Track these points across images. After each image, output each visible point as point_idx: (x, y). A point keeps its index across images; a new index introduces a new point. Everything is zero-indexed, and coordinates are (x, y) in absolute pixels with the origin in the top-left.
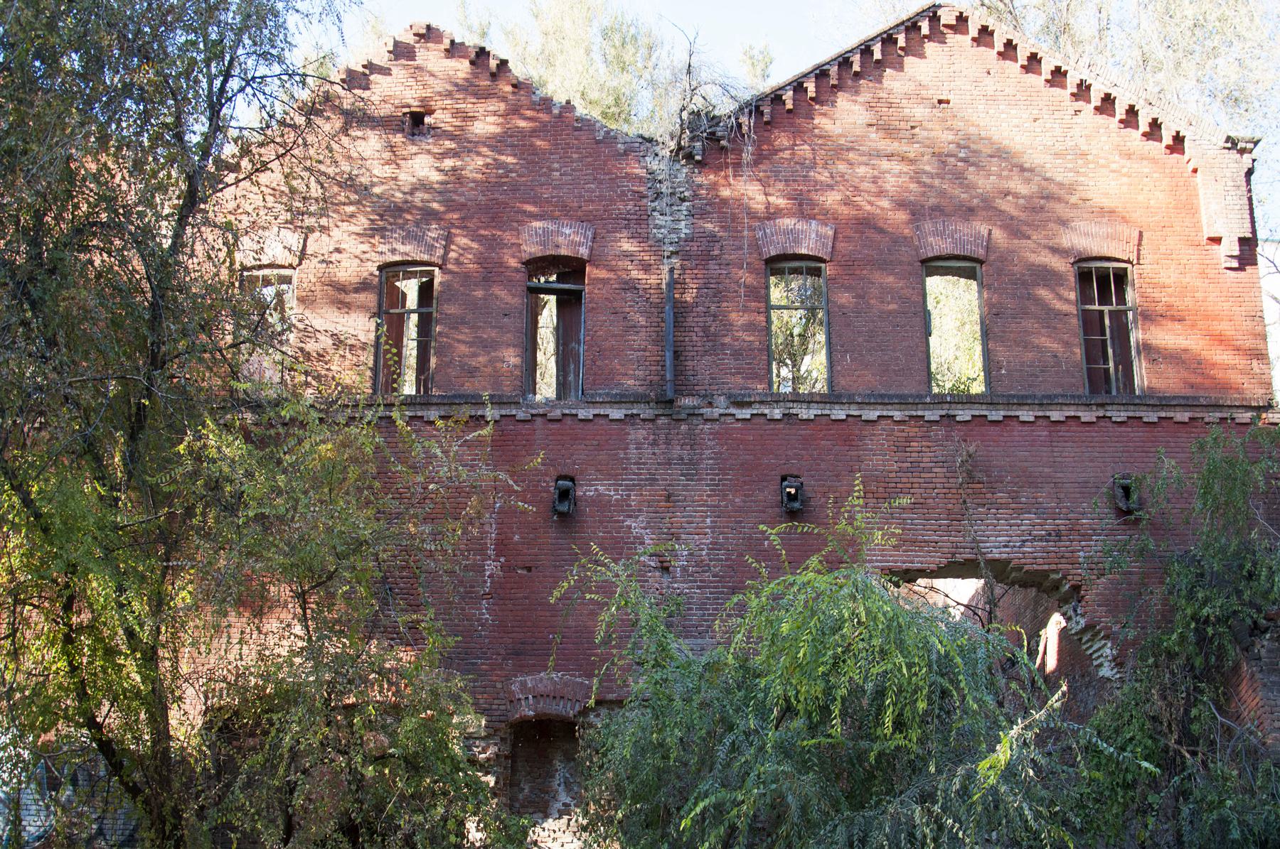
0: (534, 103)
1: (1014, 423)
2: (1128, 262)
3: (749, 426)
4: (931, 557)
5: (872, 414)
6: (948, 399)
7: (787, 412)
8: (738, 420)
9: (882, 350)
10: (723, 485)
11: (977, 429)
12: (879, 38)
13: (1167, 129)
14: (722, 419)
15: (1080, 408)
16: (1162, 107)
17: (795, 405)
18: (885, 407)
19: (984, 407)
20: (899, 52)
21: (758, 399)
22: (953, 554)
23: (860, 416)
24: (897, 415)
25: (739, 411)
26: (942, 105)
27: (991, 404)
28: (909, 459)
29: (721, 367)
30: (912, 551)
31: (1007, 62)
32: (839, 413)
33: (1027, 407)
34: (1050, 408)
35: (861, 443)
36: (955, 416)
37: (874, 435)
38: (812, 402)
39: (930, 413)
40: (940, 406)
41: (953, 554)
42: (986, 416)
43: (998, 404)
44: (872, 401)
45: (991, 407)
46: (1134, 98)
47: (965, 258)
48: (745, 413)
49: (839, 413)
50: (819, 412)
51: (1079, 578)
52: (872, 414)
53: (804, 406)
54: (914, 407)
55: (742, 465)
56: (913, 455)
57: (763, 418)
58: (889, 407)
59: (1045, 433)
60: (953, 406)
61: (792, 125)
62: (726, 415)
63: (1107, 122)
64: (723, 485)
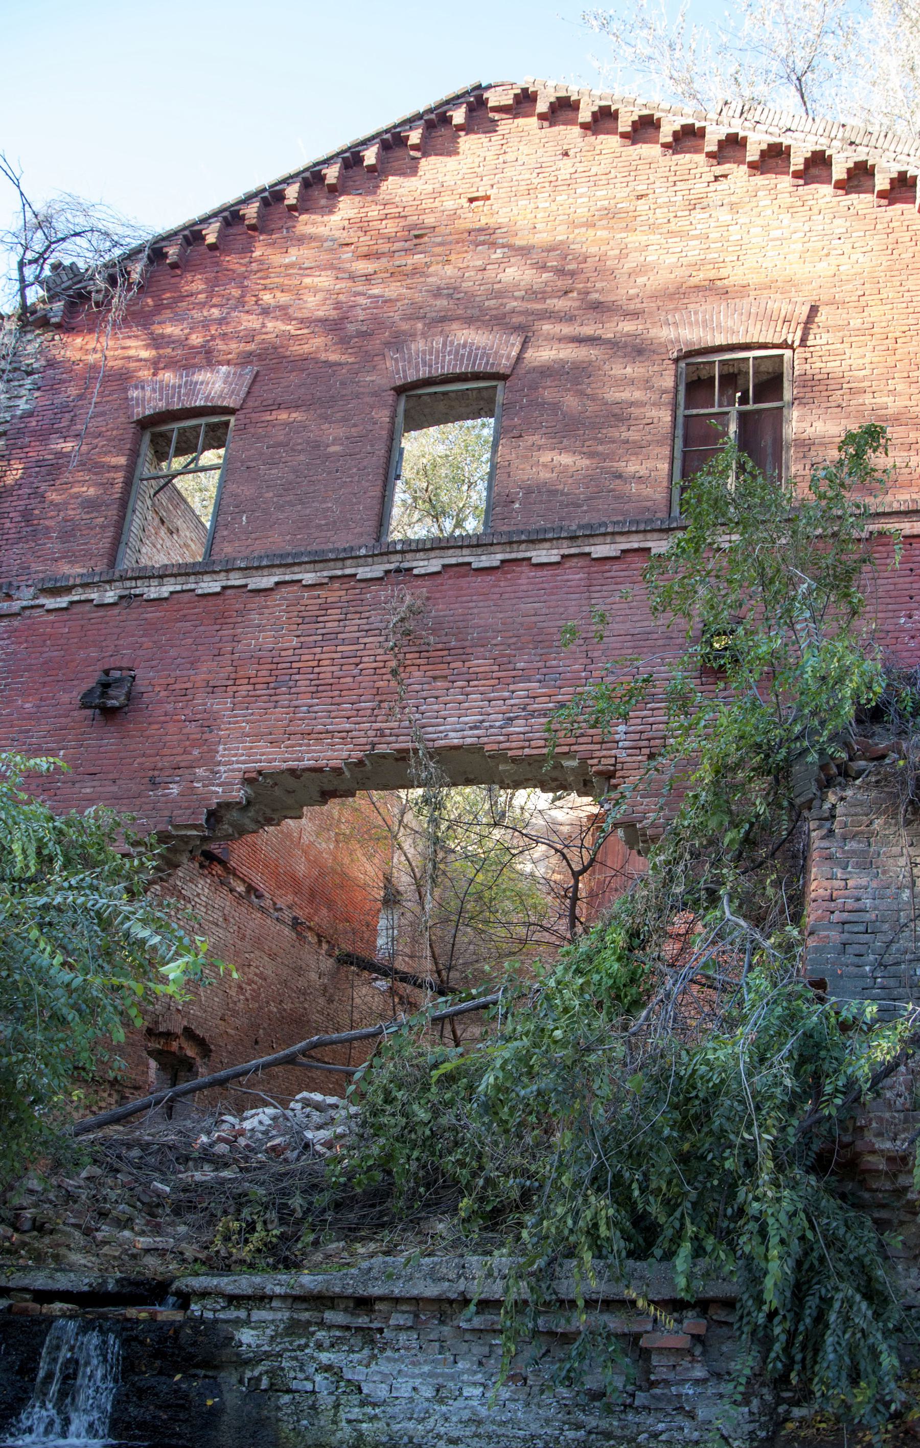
0: (216, 437)
1: (525, 568)
2: (785, 345)
3: (66, 617)
4: (335, 751)
5: (267, 581)
6: (399, 547)
7: (126, 592)
8: (48, 611)
9: (303, 503)
10: (12, 690)
11: (450, 582)
12: (377, 140)
13: (883, 171)
14: (28, 612)
15: (649, 536)
16: (873, 143)
17: (139, 583)
18: (288, 571)
19: (466, 551)
20: (412, 153)
21: (78, 581)
22: (374, 745)
23: (246, 586)
24: (309, 578)
25: (52, 600)
26: (475, 204)
27: (478, 546)
28: (319, 631)
29: (39, 554)
30: (301, 745)
31: (601, 137)
32: (210, 585)
33: (547, 545)
34: (592, 541)
35: (239, 619)
36: (411, 569)
37: (267, 607)
38: (167, 576)
39: (367, 569)
40: (385, 558)
41: (374, 745)
42: (469, 564)
43: (492, 545)
44: (264, 563)
45: (479, 551)
46: (823, 140)
47: (477, 376)
48: (62, 602)
49: (210, 585)
50: (178, 588)
51: (612, 761)
52: (267, 581)
53: (154, 582)
54: (339, 564)
55: (45, 663)
56: (328, 625)
57: (89, 605)
58: (296, 569)
59: (581, 575)
60: (409, 556)
61: (217, 264)
62: (32, 607)
63: (775, 181)
64: (12, 690)
